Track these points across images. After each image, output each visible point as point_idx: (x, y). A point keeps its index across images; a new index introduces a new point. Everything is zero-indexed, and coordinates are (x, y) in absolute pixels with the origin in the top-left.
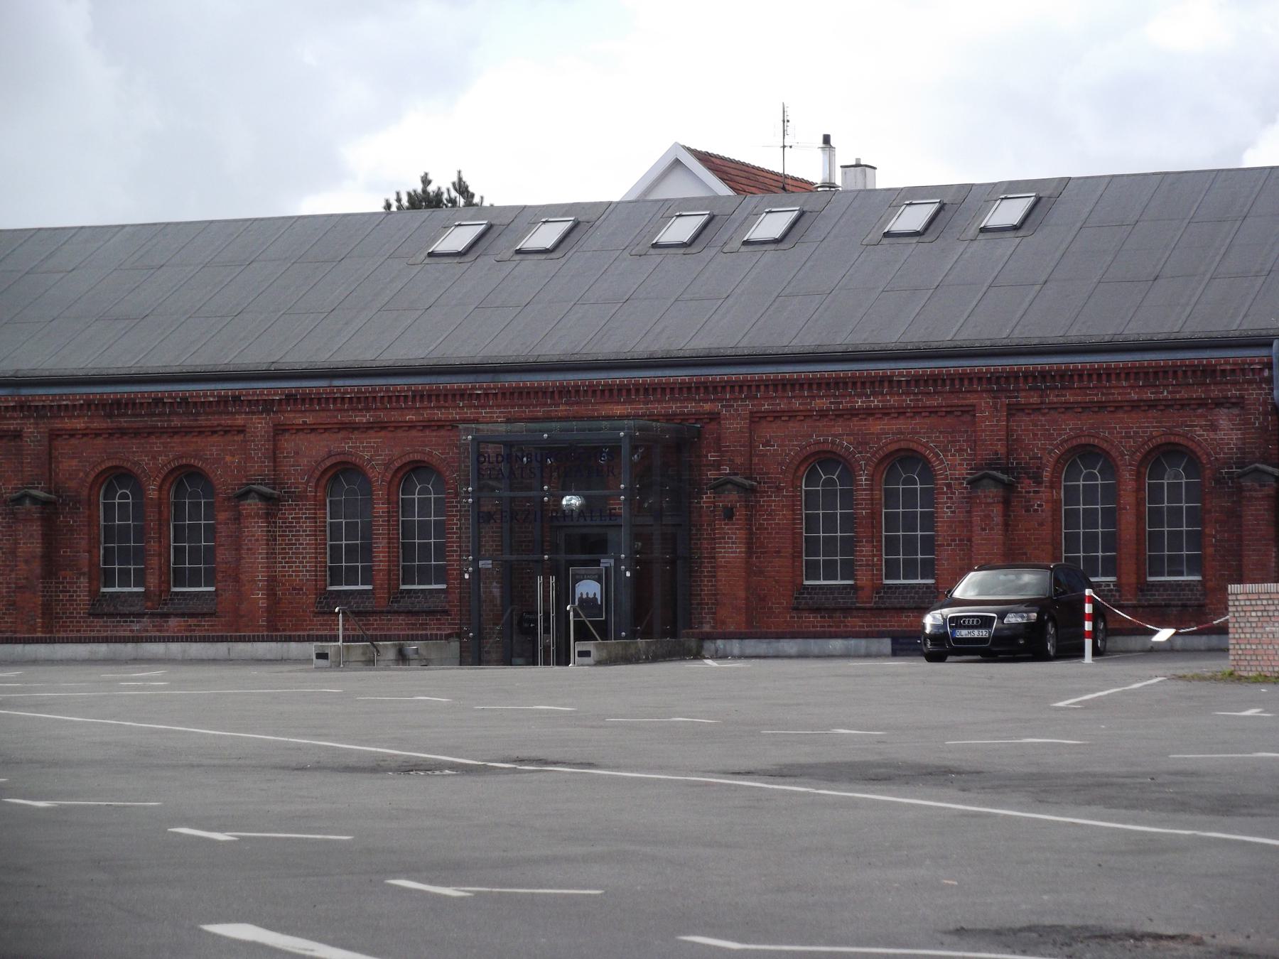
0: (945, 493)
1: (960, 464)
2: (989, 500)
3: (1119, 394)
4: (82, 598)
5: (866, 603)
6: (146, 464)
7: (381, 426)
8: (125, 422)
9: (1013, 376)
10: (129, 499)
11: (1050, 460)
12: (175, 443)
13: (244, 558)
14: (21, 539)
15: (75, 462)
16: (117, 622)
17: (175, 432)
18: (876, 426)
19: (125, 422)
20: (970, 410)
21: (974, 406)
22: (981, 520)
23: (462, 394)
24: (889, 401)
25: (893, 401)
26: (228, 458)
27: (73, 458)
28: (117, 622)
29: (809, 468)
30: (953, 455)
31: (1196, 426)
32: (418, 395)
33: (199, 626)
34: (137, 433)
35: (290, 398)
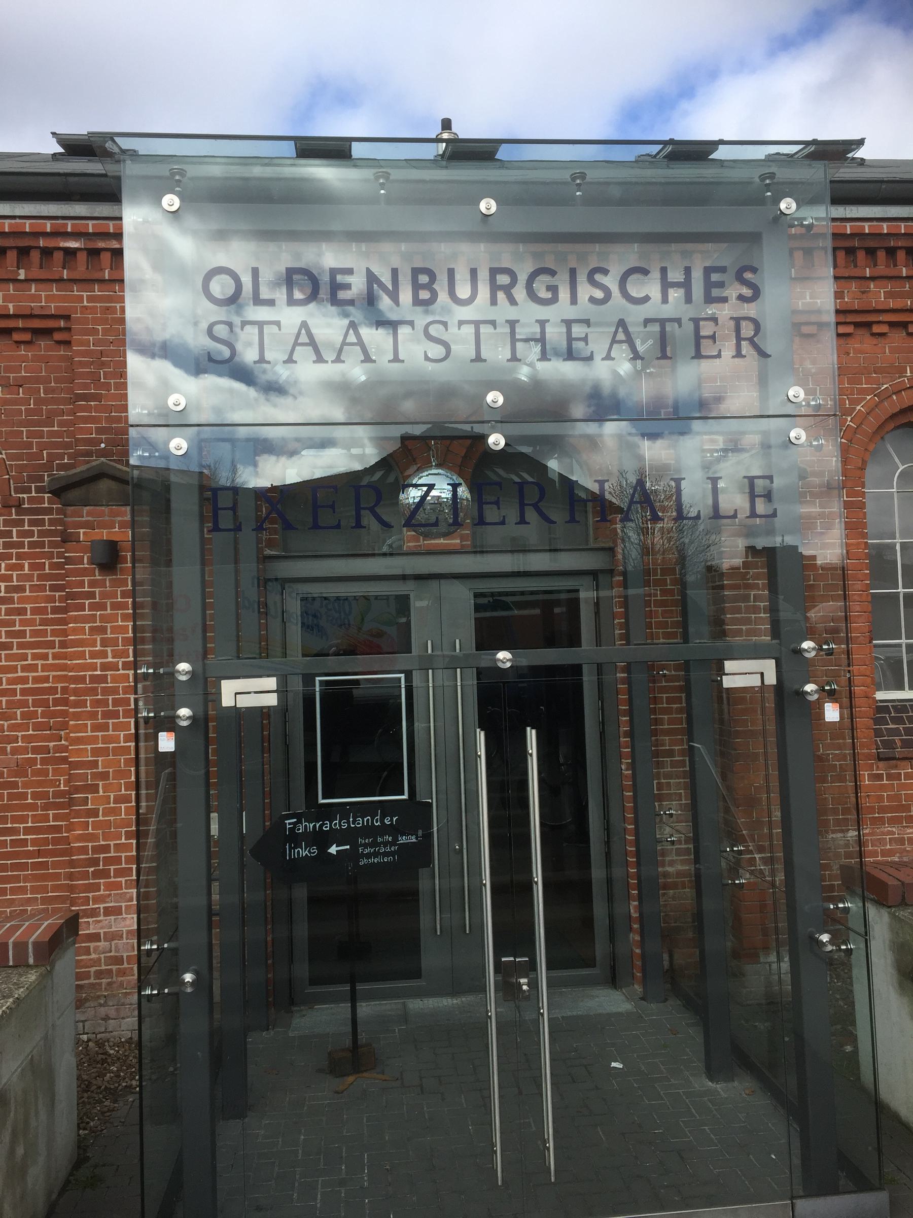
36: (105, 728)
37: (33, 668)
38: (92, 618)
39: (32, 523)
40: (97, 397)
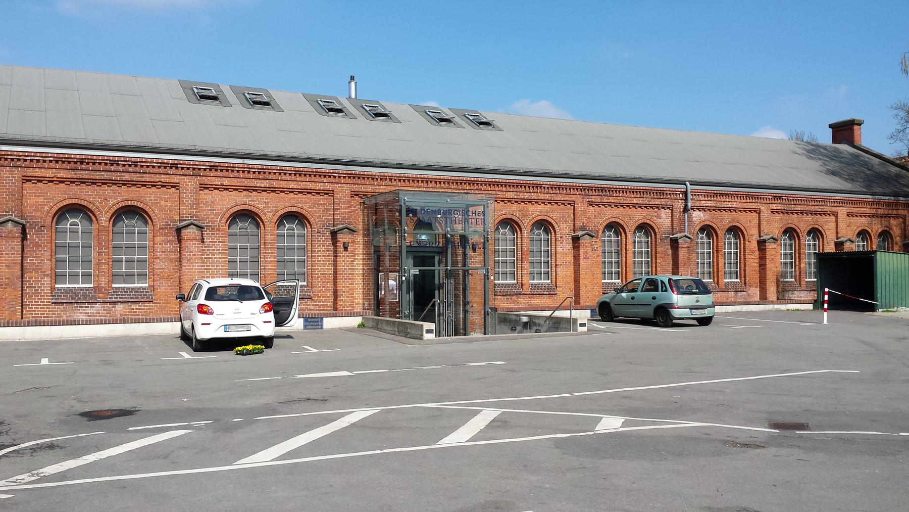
0: (560, 241)
1: (566, 228)
2: (587, 245)
3: (630, 200)
4: (45, 291)
5: (526, 291)
6: (99, 203)
7: (273, 190)
8: (87, 174)
9: (591, 189)
10: (78, 226)
11: (601, 228)
12: (122, 191)
13: (185, 266)
14: (4, 251)
15: (40, 200)
16: (75, 307)
17: (125, 183)
18: (530, 207)
19: (87, 174)
20: (572, 204)
21: (574, 201)
22: (584, 254)
23: (325, 175)
24: (540, 196)
25: (541, 196)
26: (163, 203)
27: (39, 196)
28: (75, 307)
29: (229, 221)
30: (563, 223)
31: (654, 216)
32: (298, 173)
33: (140, 309)
34: (94, 182)
35: (213, 167)
36: (344, 282)
37: (323, 269)
38: (342, 258)
39: (323, 236)
40: (339, 209)
